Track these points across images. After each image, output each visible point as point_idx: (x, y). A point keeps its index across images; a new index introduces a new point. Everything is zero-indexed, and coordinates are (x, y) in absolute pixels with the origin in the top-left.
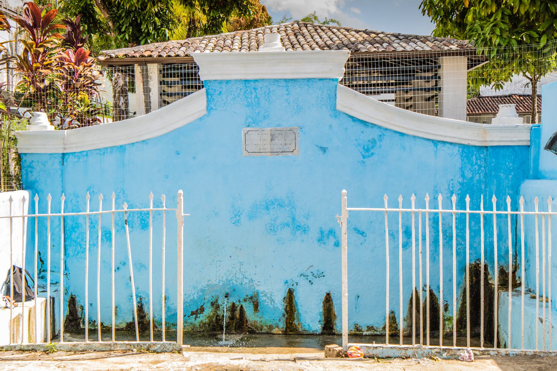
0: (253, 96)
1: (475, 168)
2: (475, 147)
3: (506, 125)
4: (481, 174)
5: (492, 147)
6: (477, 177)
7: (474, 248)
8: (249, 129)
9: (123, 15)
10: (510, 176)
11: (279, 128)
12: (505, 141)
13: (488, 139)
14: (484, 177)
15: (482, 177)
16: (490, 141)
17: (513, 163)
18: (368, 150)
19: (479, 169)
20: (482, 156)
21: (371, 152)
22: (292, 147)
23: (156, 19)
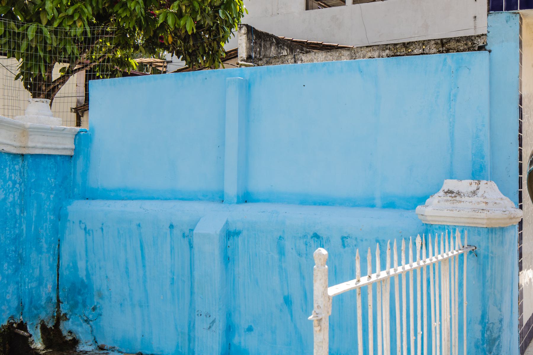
1: (9, 185)
2: (9, 154)
3: (53, 126)
4: (16, 194)
5: (32, 155)
6: (11, 199)
7: (7, 301)
10: (52, 196)
12: (48, 148)
13: (30, 144)
14: (19, 198)
15: (16, 198)
16: (33, 147)
17: (55, 179)
19: (14, 187)
20: (17, 167)
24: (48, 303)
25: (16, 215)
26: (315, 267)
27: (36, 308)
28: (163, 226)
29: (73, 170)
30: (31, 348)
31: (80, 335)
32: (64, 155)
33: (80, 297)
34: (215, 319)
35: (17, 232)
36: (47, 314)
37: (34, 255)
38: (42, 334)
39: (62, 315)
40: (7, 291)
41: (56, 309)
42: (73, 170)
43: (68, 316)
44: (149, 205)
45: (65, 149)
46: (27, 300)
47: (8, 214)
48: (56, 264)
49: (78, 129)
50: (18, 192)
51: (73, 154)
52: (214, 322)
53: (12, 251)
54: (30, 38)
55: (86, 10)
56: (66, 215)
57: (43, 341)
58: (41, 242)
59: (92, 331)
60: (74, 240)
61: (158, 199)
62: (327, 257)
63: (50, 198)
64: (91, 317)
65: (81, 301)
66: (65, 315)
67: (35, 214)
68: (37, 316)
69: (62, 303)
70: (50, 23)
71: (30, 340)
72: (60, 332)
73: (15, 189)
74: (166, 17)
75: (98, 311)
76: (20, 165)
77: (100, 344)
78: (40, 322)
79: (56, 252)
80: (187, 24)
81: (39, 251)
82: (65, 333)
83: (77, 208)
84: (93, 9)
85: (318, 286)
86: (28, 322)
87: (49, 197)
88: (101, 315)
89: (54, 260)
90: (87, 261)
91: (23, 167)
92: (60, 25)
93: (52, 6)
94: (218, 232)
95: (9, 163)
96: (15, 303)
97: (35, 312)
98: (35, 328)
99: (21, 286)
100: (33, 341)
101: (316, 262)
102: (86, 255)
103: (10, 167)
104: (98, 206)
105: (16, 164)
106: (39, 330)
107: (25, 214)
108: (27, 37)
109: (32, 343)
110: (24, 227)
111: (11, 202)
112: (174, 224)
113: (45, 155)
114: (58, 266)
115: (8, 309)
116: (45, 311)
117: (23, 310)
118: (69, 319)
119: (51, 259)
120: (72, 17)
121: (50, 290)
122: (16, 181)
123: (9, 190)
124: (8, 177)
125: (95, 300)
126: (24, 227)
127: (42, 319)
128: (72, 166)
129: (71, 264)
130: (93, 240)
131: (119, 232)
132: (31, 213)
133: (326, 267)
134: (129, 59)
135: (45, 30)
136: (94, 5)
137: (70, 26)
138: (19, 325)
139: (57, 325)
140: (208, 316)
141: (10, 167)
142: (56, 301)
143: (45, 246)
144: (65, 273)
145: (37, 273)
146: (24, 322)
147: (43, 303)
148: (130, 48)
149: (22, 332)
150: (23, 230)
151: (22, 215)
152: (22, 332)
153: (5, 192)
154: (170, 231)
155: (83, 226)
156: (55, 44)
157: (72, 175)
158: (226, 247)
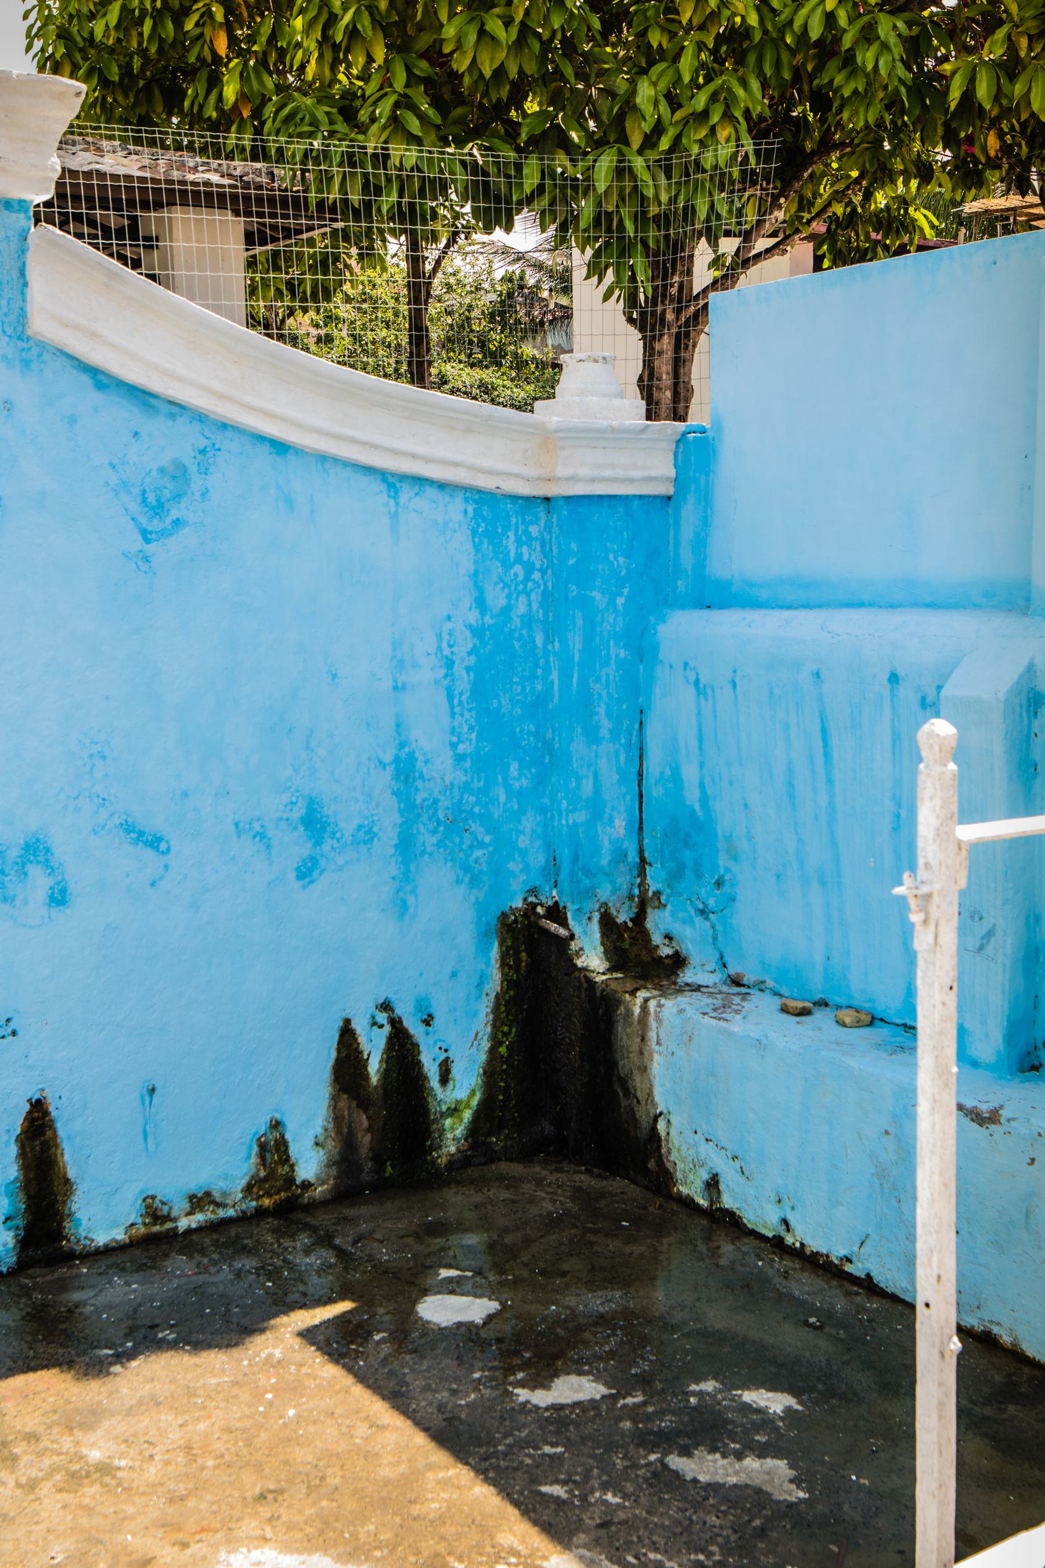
1: (516, 575)
2: (514, 498)
3: (615, 423)
6: (521, 608)
10: (620, 601)
13: (561, 471)
15: (535, 606)
16: (567, 479)
17: (628, 557)
18: (158, 509)
19: (527, 578)
20: (534, 530)
21: (174, 514)
24: (617, 862)
25: (535, 647)
26: (922, 766)
27: (589, 874)
28: (874, 676)
29: (672, 532)
30: (575, 965)
31: (690, 946)
32: (649, 496)
33: (687, 853)
34: (994, 926)
35: (539, 687)
36: (615, 890)
37: (579, 746)
38: (602, 937)
39: (650, 894)
40: (521, 828)
41: (638, 880)
42: (672, 532)
43: (663, 899)
44: (846, 624)
45: (649, 479)
46: (565, 854)
47: (516, 644)
48: (635, 769)
49: (681, 426)
50: (540, 591)
51: (671, 491)
52: (990, 933)
53: (529, 733)
54: (601, 186)
55: (740, 92)
56: (656, 648)
57: (606, 952)
58: (597, 713)
59: (715, 938)
60: (673, 709)
61: (871, 605)
62: (954, 744)
63: (614, 605)
64: (711, 903)
65: (690, 863)
66: (657, 894)
67: (578, 646)
68: (590, 892)
69: (651, 865)
70: (650, 141)
71: (574, 946)
72: (645, 935)
73: (530, 584)
74: (972, 81)
75: (726, 889)
76: (542, 523)
77: (732, 970)
78: (597, 906)
79: (635, 740)
80: (1034, 90)
81: (593, 736)
82: (657, 939)
83: (682, 630)
84: (764, 85)
85: (928, 817)
86: (569, 905)
87: (612, 603)
88: (734, 900)
89: (629, 758)
90: (702, 765)
91: (548, 528)
92: (677, 140)
93: (653, 93)
94: (1002, 696)
95: (514, 520)
96: (539, 859)
97: (586, 882)
98: (585, 921)
99: (552, 818)
100: (581, 949)
101: (924, 754)
102: (700, 749)
103: (517, 530)
104: (726, 624)
105: (532, 523)
106: (595, 927)
107: (557, 644)
108: (595, 189)
109: (579, 953)
110: (555, 676)
111: (522, 616)
112: (901, 672)
113: (601, 497)
114: (640, 774)
115: (521, 871)
116: (611, 882)
117: (558, 875)
118: (665, 906)
119: (622, 758)
120: (704, 115)
121: (622, 832)
122: (533, 563)
123: (517, 585)
124: (512, 554)
125: (721, 863)
126: (555, 676)
127: (603, 900)
128: (671, 521)
129: (668, 772)
130: (714, 711)
131: (771, 692)
132: (570, 642)
133: (952, 766)
134: (911, 210)
135: (638, 163)
136: (768, 71)
137: (702, 143)
138: (549, 909)
139: (639, 918)
140: (977, 918)
141: (517, 530)
142: (638, 860)
143: (606, 724)
144: (654, 793)
145: (587, 788)
146: (561, 905)
147: (604, 862)
148: (893, 182)
149: (553, 927)
150: (552, 682)
151: (550, 647)
152: (553, 927)
153: (506, 591)
154: (892, 690)
155: (692, 677)
156: (664, 198)
157: (671, 545)
158: (1028, 736)
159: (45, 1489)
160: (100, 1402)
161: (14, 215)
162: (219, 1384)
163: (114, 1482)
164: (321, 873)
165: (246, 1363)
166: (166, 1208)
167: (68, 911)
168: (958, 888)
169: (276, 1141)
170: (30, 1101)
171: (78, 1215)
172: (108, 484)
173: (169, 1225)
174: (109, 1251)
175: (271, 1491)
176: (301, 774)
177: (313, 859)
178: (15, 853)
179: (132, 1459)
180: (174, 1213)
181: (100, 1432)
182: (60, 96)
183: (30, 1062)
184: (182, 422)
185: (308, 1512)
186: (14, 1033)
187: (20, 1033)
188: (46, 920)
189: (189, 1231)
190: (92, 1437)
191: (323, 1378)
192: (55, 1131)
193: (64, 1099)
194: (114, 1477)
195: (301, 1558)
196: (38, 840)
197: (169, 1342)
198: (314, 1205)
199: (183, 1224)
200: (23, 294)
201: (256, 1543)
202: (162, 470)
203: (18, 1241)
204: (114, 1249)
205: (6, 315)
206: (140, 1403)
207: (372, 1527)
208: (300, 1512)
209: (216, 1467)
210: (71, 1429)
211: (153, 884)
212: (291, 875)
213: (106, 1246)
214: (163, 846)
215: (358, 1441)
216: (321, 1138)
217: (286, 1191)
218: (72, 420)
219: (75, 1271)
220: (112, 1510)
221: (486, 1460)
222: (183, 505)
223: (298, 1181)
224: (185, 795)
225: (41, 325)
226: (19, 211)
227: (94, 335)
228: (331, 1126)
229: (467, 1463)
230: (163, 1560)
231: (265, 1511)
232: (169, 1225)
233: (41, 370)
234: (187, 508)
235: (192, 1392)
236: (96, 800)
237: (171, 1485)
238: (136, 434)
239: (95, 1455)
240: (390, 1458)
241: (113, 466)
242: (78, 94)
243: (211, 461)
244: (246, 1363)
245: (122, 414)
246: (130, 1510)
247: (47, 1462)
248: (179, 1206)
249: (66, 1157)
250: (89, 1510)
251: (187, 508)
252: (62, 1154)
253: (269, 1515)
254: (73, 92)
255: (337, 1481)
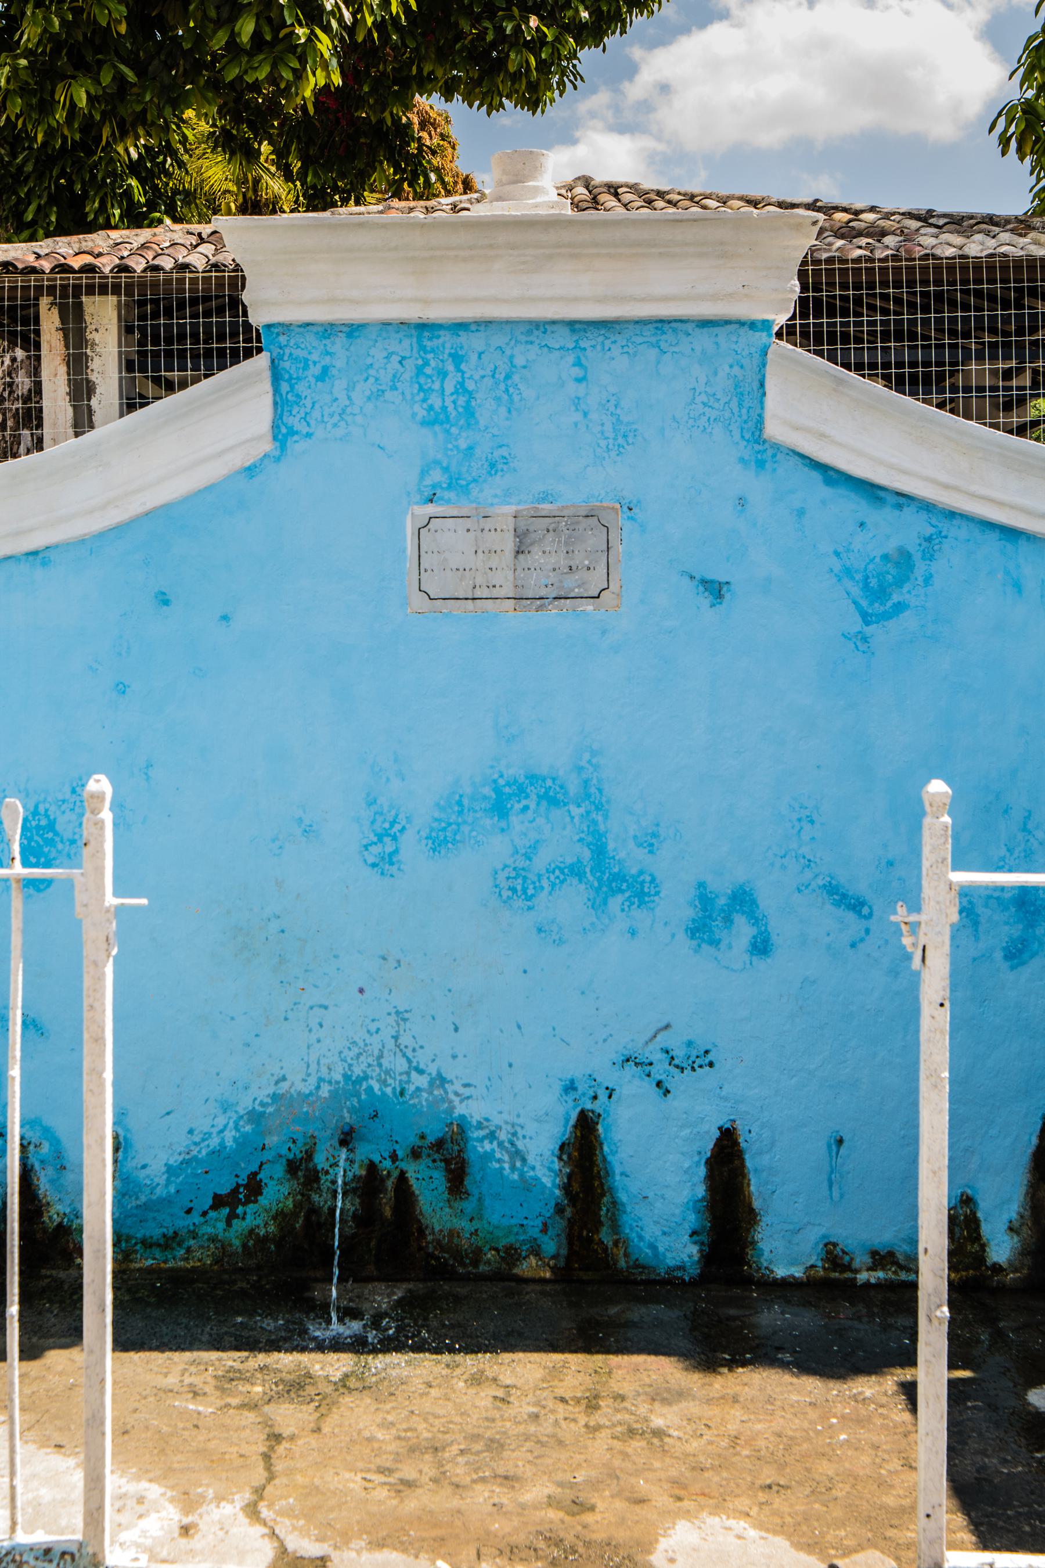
0: (449, 387)
8: (431, 509)
9: (29, 168)
11: (546, 507)
18: (881, 593)
21: (896, 598)
22: (596, 581)
23: (134, 182)
159: (605, 1433)
160: (692, 1389)
161: (758, 334)
162: (798, 1402)
163: (658, 1444)
164: (1032, 957)
165: (835, 1392)
166: (847, 1258)
167: (769, 961)
168: (950, 922)
169: (966, 1216)
170: (720, 1128)
171: (760, 1245)
172: (832, 570)
173: (848, 1275)
174: (787, 1285)
175: (779, 1485)
176: (1016, 855)
177: (1023, 941)
178: (722, 901)
179: (685, 1433)
180: (856, 1264)
181: (675, 1408)
182: (798, 227)
183: (723, 1093)
184: (909, 513)
185: (798, 1508)
186: (711, 1064)
187: (717, 1065)
188: (748, 966)
189: (867, 1285)
190: (665, 1410)
191: (892, 1420)
192: (743, 1161)
193: (753, 1134)
194: (662, 1440)
195: (764, 1534)
196: (745, 892)
197: (783, 1362)
198: (1003, 1290)
199: (863, 1277)
200: (762, 403)
201: (737, 1515)
202: (886, 557)
203: (702, 1256)
204: (790, 1284)
205: (745, 422)
206: (723, 1398)
207: (843, 1533)
208: (791, 1505)
209: (748, 1457)
210: (653, 1400)
211: (853, 945)
212: (999, 955)
213: (783, 1279)
214: (865, 911)
215: (883, 1472)
216: (1016, 1225)
217: (974, 1270)
218: (801, 513)
219: (747, 1294)
220: (642, 1461)
221: (987, 1517)
222: (905, 590)
223: (989, 1263)
224: (890, 864)
225: (774, 430)
226: (762, 330)
227: (822, 436)
228: (1027, 1214)
229: (968, 1515)
230: (654, 1503)
231: (762, 1496)
232: (848, 1275)
233: (774, 470)
234: (909, 592)
235: (770, 1400)
236: (802, 860)
237: (702, 1459)
238: (861, 525)
239: (658, 1422)
240: (901, 1492)
241: (837, 554)
242: (815, 223)
243: (936, 548)
244: (835, 1392)
245: (850, 506)
246: (657, 1465)
247: (619, 1416)
248: (861, 1259)
249: (752, 1188)
250: (625, 1456)
251: (909, 592)
252: (749, 1185)
253: (764, 1500)
254: (810, 221)
255: (839, 1494)
